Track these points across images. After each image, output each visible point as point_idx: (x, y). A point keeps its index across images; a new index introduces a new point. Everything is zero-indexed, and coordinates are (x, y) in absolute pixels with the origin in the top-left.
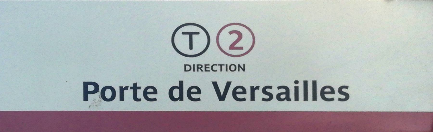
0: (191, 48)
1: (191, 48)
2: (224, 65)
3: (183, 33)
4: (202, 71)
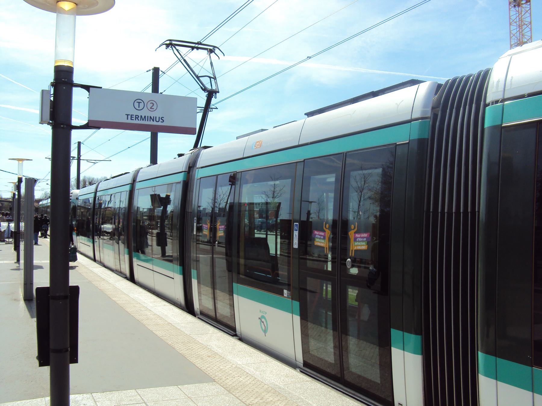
0: (139, 107)
1: (139, 107)
2: (129, 115)
3: (137, 102)
4: (138, 120)
